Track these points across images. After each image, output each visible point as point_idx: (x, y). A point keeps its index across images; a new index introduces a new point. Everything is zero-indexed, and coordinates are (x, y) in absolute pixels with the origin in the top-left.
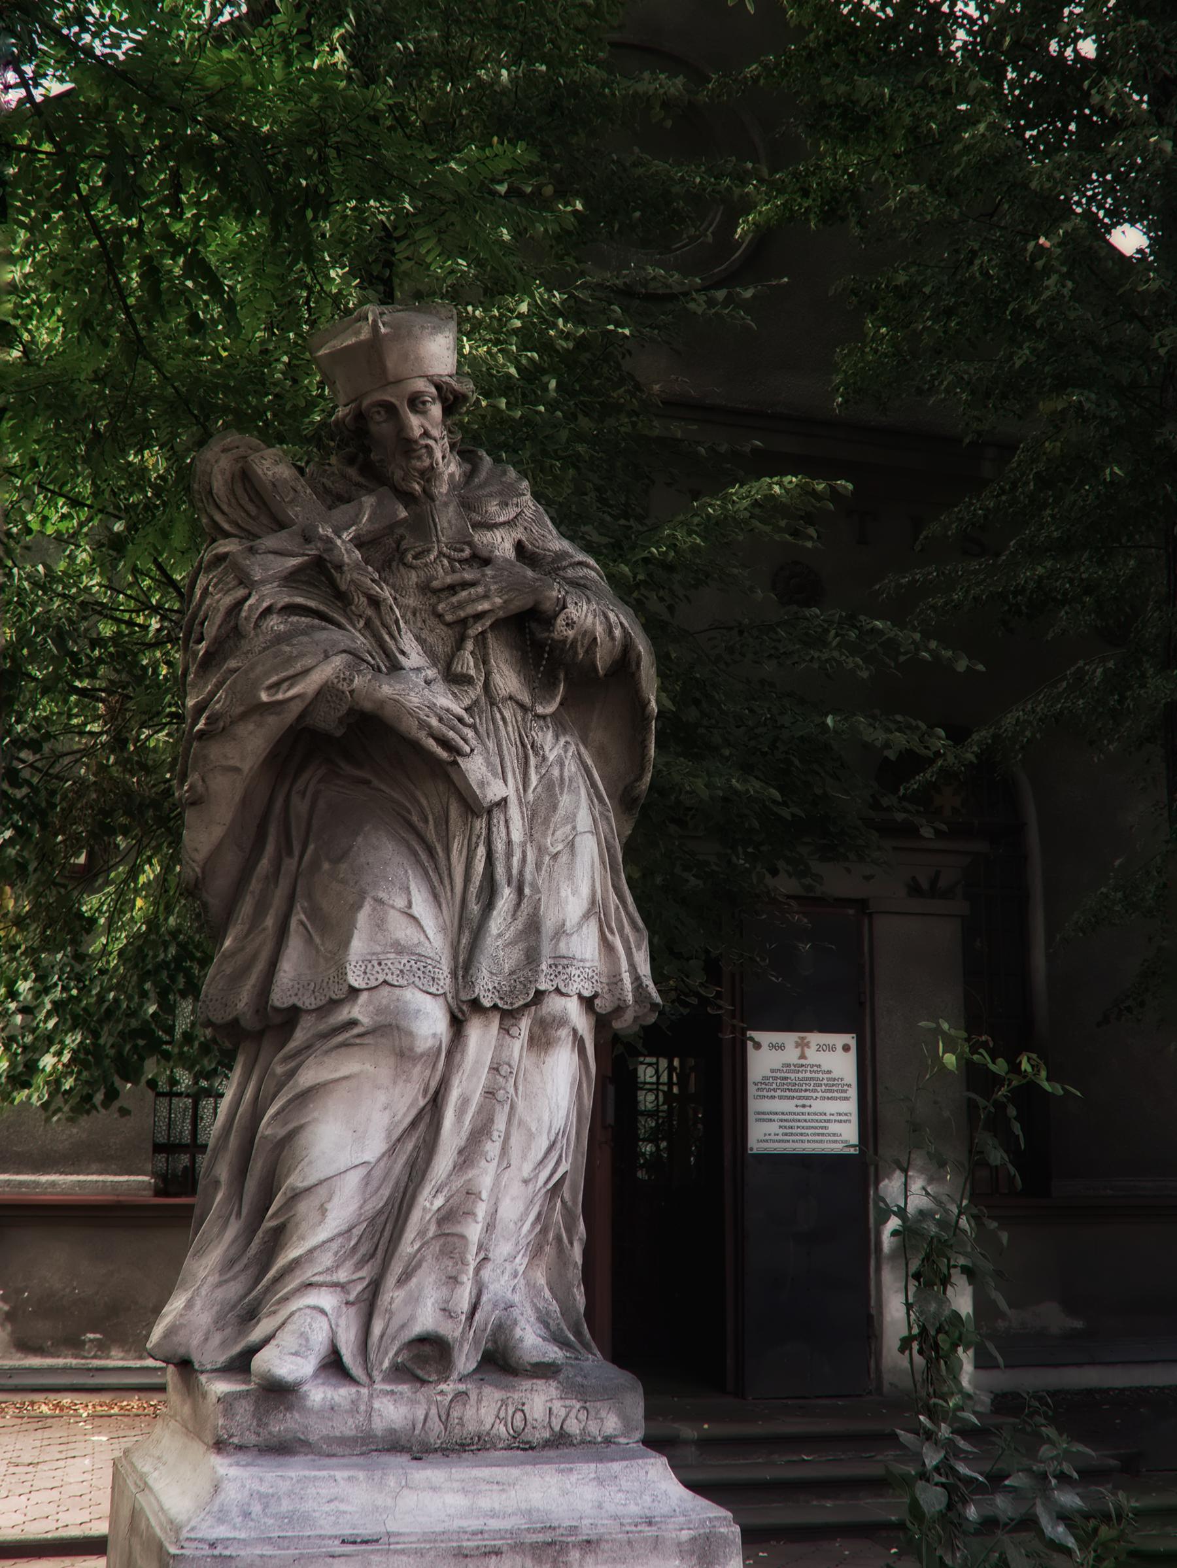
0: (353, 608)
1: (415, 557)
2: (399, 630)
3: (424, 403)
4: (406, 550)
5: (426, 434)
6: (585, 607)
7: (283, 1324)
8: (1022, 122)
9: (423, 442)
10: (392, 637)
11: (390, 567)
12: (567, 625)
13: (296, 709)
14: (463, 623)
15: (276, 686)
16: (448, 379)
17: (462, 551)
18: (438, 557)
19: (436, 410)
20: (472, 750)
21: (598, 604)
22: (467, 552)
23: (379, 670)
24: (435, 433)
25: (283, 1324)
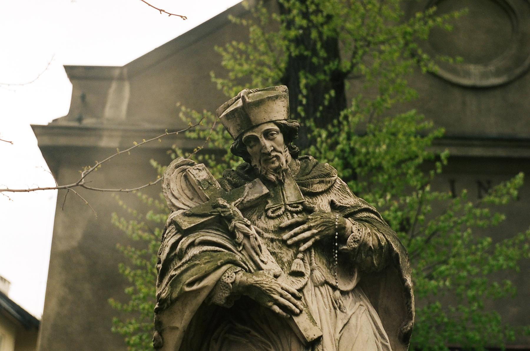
0: (236, 240)
1: (273, 212)
2: (261, 251)
3: (272, 134)
4: (269, 209)
5: (275, 150)
6: (364, 232)
7: (328, 301)
8: (336, 244)
9: (274, 154)
10: (257, 254)
11: (260, 218)
12: (354, 241)
13: (204, 295)
14: (297, 244)
15: (191, 284)
16: (284, 122)
17: (298, 207)
18: (285, 211)
19: (280, 138)
20: (301, 311)
21: (371, 229)
22: (300, 208)
23: (250, 271)
24: (279, 149)
25: (328, 301)
